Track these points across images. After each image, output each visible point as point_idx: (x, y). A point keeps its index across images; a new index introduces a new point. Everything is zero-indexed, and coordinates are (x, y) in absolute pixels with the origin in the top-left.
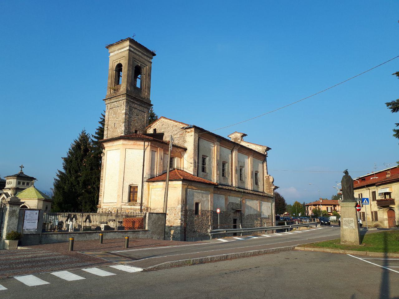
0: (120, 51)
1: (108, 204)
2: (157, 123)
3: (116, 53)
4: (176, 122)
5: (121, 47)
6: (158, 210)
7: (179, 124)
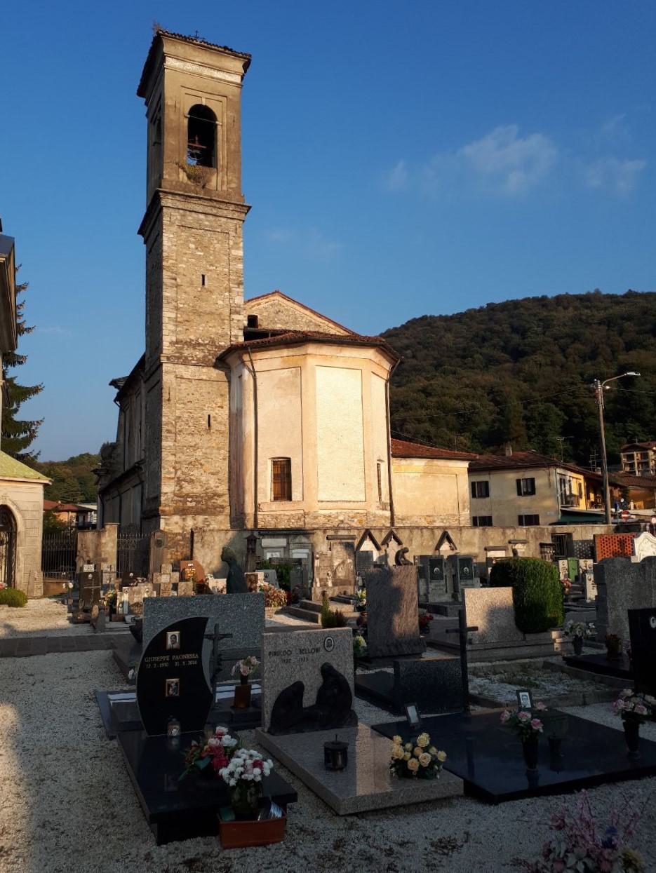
0: (206, 72)
1: (339, 504)
2: (261, 301)
3: (189, 67)
4: (321, 316)
5: (210, 62)
6: (415, 519)
7: (327, 323)
